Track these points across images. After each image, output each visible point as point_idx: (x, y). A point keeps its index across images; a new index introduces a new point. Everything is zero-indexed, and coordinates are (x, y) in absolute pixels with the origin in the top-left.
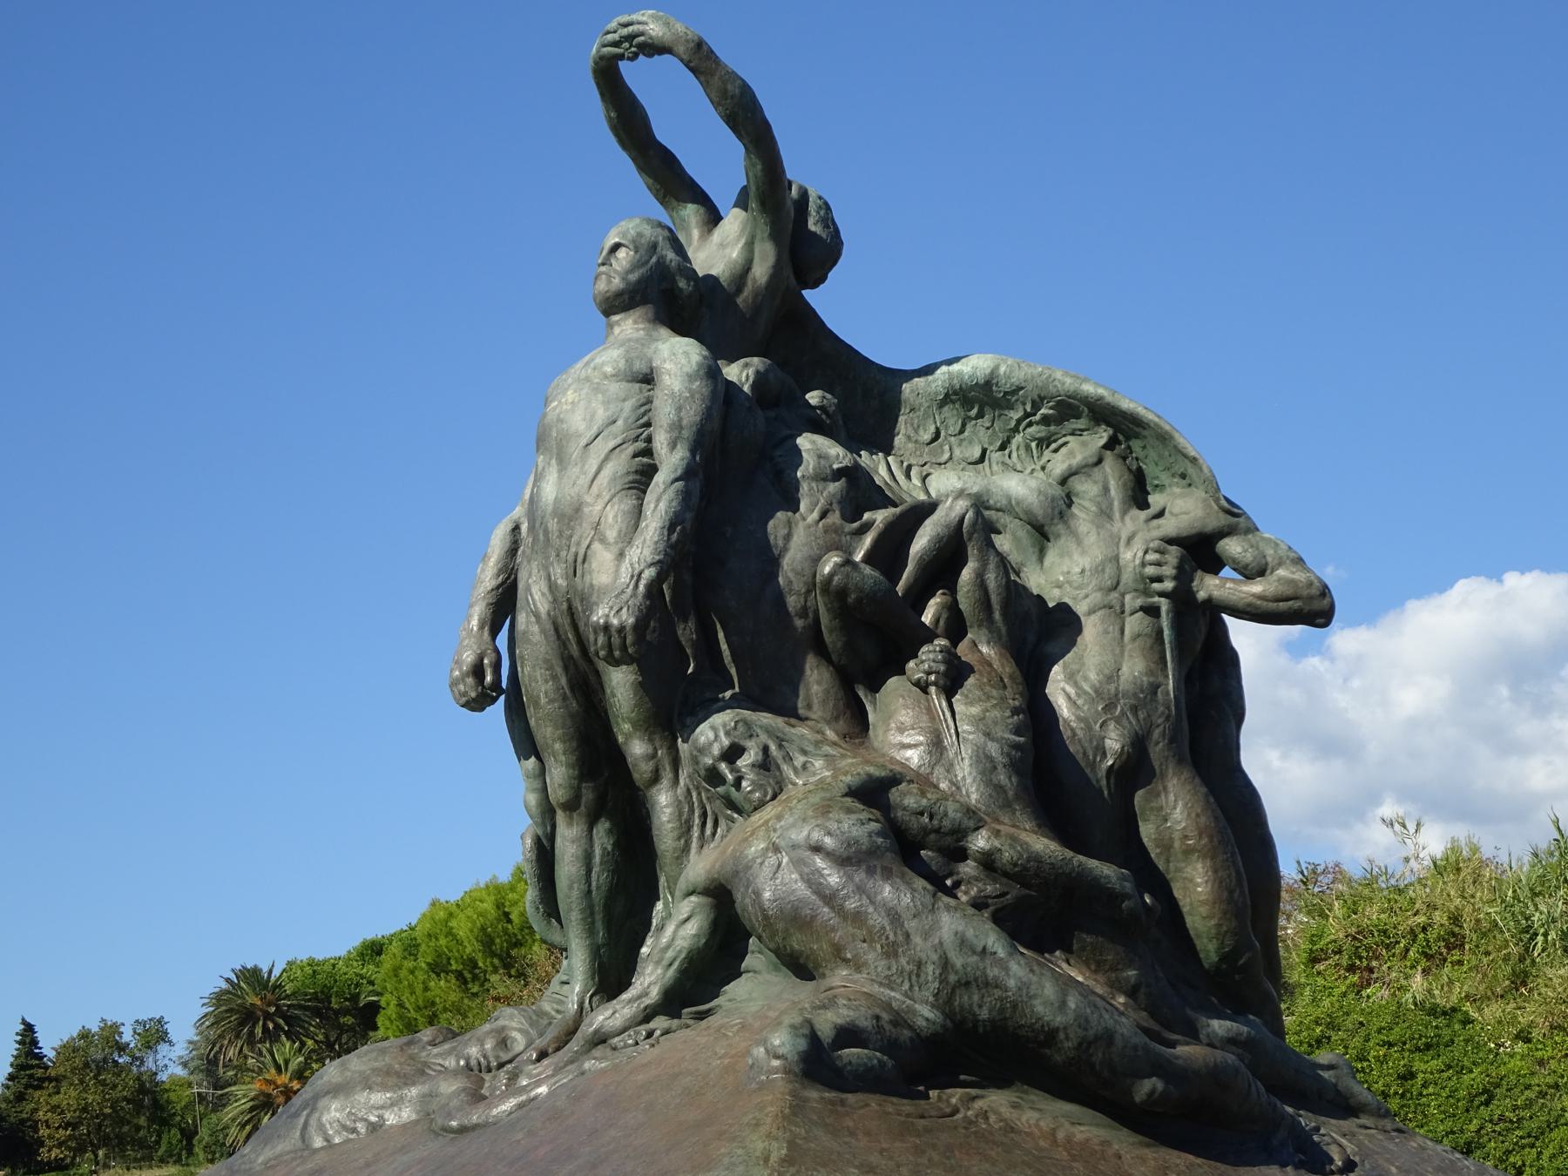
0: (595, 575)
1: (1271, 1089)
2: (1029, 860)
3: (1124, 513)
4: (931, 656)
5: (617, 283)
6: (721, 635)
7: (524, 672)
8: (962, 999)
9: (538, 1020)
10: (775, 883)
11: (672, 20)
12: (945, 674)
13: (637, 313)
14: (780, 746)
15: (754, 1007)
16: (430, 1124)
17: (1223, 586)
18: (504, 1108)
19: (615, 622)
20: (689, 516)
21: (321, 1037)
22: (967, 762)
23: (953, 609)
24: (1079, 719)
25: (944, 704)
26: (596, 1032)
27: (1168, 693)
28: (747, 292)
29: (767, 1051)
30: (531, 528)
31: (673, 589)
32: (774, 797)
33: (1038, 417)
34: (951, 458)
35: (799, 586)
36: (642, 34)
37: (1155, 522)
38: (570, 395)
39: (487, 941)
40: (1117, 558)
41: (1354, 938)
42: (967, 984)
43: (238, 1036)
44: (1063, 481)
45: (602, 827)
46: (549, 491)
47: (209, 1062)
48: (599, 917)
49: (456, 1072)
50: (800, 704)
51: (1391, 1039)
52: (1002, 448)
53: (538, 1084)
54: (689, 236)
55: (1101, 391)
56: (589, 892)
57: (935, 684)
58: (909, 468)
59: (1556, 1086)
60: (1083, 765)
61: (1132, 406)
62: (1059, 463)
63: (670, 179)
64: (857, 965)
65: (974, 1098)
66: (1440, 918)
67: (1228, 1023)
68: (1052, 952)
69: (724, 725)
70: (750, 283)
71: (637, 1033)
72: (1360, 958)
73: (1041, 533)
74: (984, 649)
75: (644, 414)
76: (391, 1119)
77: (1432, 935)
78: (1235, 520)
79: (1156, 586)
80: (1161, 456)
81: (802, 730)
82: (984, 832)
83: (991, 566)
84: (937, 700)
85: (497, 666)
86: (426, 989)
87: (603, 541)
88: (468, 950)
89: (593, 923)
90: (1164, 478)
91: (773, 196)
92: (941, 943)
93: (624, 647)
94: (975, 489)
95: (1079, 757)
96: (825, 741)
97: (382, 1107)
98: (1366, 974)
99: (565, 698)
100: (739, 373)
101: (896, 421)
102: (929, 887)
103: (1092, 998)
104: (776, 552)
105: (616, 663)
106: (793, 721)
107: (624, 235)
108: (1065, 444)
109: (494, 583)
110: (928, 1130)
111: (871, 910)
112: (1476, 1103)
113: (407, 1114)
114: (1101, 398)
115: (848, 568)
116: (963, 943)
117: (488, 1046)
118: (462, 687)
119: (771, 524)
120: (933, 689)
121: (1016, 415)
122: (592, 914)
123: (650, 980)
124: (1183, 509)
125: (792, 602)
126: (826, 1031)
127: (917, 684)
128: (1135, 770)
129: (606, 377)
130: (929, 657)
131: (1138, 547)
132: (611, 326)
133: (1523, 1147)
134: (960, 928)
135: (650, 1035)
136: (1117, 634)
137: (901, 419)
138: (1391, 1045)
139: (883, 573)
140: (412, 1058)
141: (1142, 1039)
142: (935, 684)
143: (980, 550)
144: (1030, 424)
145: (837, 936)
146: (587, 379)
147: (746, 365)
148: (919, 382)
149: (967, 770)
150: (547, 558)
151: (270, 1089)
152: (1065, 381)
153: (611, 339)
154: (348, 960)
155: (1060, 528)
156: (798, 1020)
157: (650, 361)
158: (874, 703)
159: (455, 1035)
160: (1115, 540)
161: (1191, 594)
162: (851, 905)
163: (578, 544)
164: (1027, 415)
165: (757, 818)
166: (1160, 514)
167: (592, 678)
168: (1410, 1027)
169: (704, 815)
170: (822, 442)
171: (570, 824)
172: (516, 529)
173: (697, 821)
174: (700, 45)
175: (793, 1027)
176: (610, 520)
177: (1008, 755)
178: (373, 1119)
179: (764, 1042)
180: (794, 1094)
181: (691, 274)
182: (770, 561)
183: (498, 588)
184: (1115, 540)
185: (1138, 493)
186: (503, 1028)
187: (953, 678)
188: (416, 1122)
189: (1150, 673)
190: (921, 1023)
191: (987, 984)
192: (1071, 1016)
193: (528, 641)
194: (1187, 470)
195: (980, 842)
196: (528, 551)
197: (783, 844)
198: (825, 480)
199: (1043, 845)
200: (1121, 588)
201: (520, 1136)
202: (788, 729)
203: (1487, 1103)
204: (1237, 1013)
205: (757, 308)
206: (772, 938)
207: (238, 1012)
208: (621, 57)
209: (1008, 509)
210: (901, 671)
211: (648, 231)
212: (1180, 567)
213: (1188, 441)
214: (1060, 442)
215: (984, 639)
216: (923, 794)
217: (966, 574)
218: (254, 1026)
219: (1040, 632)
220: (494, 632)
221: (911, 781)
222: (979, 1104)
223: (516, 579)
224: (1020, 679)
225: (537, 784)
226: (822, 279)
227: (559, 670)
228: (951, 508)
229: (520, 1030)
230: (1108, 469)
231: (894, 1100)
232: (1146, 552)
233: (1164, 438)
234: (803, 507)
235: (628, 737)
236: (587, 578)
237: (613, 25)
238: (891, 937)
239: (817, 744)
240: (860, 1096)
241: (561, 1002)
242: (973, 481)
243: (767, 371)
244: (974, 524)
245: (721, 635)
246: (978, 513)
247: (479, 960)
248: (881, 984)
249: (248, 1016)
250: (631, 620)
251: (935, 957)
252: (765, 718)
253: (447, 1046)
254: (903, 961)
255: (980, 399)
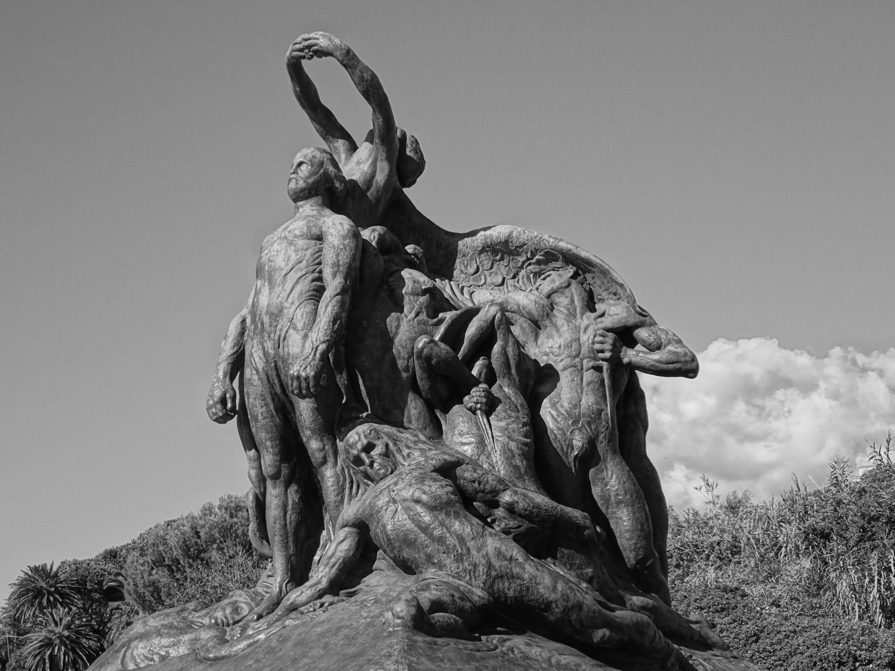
0: (290, 348)
1: (666, 635)
2: (534, 507)
3: (582, 314)
4: (478, 394)
5: (301, 184)
6: (361, 381)
7: (250, 402)
8: (500, 585)
9: (256, 598)
10: (393, 520)
11: (333, 37)
12: (486, 404)
13: (312, 201)
14: (395, 444)
15: (381, 590)
16: (197, 656)
17: (638, 355)
18: (240, 647)
19: (303, 374)
20: (344, 315)
21: (80, 605)
22: (498, 453)
23: (489, 368)
24: (559, 429)
25: (485, 420)
26: (292, 604)
27: (607, 415)
28: (373, 189)
29: (393, 614)
30: (253, 321)
31: (335, 356)
32: (392, 473)
33: (534, 260)
34: (485, 283)
35: (404, 354)
36: (316, 45)
37: (600, 320)
38: (276, 247)
39: (186, 548)
40: (579, 339)
41: (679, 549)
42: (502, 577)
43: (32, 605)
44: (549, 296)
45: (293, 488)
46: (264, 300)
47: (15, 620)
48: (291, 539)
49: (210, 627)
50: (405, 420)
51: (702, 605)
52: (514, 277)
53: (259, 633)
54: (340, 157)
55: (570, 246)
56: (286, 525)
57: (480, 409)
58: (463, 288)
59: (795, 632)
60: (561, 454)
61: (587, 254)
62: (546, 286)
63: (328, 124)
64: (441, 566)
65: (506, 640)
66: (727, 537)
67: (642, 598)
68: (545, 558)
69: (364, 432)
70: (374, 184)
71: (315, 604)
72: (683, 560)
73: (536, 325)
74: (506, 390)
75: (318, 258)
76: (173, 653)
77: (723, 547)
78: (644, 319)
79: (600, 355)
80: (603, 283)
81: (406, 435)
82: (508, 492)
83: (510, 344)
84: (481, 418)
85: (234, 398)
86: (150, 575)
87: (295, 328)
88: (175, 553)
89: (287, 542)
90: (604, 295)
91: (387, 135)
92: (487, 554)
93: (308, 388)
94: (500, 300)
95: (559, 450)
96: (420, 441)
97: (168, 647)
98: (686, 570)
99: (272, 416)
100: (370, 234)
101: (455, 262)
102: (480, 522)
103: (571, 584)
104: (391, 335)
105: (303, 397)
106: (401, 430)
107: (305, 157)
108: (549, 275)
109: (232, 351)
110: (482, 658)
111: (448, 535)
112: (750, 641)
113: (183, 650)
114: (570, 250)
115: (432, 345)
116: (499, 553)
117: (228, 611)
118: (214, 410)
119: (388, 320)
120: (479, 412)
121: (522, 259)
122: (287, 537)
123: (321, 574)
124: (615, 313)
125: (401, 364)
126: (426, 605)
127: (470, 409)
128: (589, 457)
129: (296, 236)
130: (476, 395)
131: (591, 331)
132: (298, 208)
133: (776, 666)
134: (498, 546)
135: (322, 605)
136: (579, 381)
137: (458, 261)
138: (702, 609)
139: (451, 347)
140: (184, 618)
141: (597, 607)
142: (480, 409)
143: (504, 335)
144: (530, 264)
145: (429, 550)
146: (286, 238)
147: (374, 230)
148: (468, 240)
149: (498, 457)
150: (263, 338)
151: (51, 636)
152: (549, 240)
153: (298, 215)
154: (97, 561)
155: (547, 322)
156: (410, 597)
157: (321, 227)
158: (445, 420)
159: (207, 606)
160: (577, 329)
161: (620, 360)
162: (437, 532)
163: (281, 330)
164: (528, 259)
165: (382, 484)
166: (603, 315)
167: (288, 405)
168: (712, 598)
169: (352, 482)
170: (416, 274)
171: (274, 487)
172: (244, 321)
173: (348, 486)
174: (349, 51)
175: (407, 601)
176: (299, 317)
177: (521, 449)
178: (163, 653)
179: (392, 609)
180: (408, 638)
181: (342, 179)
182: (388, 340)
183: (234, 354)
184: (577, 329)
185: (590, 304)
186: (236, 602)
187: (490, 406)
188: (188, 655)
189: (597, 403)
190: (476, 598)
191: (512, 577)
192: (559, 594)
193: (252, 384)
194: (617, 290)
195: (506, 497)
196: (252, 334)
197: (398, 498)
198: (417, 295)
199: (541, 499)
200: (581, 356)
201: (251, 662)
202: (399, 434)
203: (756, 641)
204: (646, 592)
205: (378, 199)
206: (392, 551)
207: (32, 591)
208: (304, 57)
209: (518, 312)
210: (461, 402)
211: (318, 154)
212: (614, 345)
213: (619, 274)
214: (546, 274)
215: (506, 384)
216: (475, 471)
217: (497, 348)
218: (42, 599)
219: (536, 381)
220: (232, 379)
221: (468, 464)
222: (508, 644)
223: (244, 350)
224: (526, 407)
225: (256, 464)
226: (414, 182)
227: (269, 401)
228: (488, 311)
229: (245, 603)
230: (574, 291)
231: (463, 641)
232: (595, 336)
233: (605, 273)
234: (405, 310)
235: (309, 438)
236: (286, 349)
237: (299, 39)
238: (460, 551)
239: (415, 443)
240: (444, 640)
241: (267, 587)
242: (499, 296)
243: (385, 234)
244: (501, 320)
245: (361, 381)
246: (503, 314)
247: (186, 563)
248: (453, 577)
249: (39, 593)
250: (313, 373)
251: (484, 562)
252: (386, 428)
253: (204, 612)
254: (466, 564)
255: (502, 250)
